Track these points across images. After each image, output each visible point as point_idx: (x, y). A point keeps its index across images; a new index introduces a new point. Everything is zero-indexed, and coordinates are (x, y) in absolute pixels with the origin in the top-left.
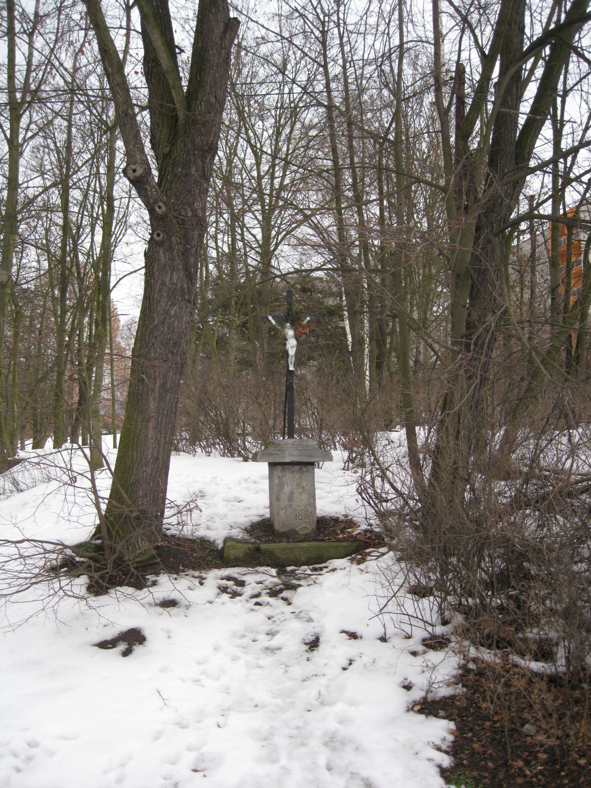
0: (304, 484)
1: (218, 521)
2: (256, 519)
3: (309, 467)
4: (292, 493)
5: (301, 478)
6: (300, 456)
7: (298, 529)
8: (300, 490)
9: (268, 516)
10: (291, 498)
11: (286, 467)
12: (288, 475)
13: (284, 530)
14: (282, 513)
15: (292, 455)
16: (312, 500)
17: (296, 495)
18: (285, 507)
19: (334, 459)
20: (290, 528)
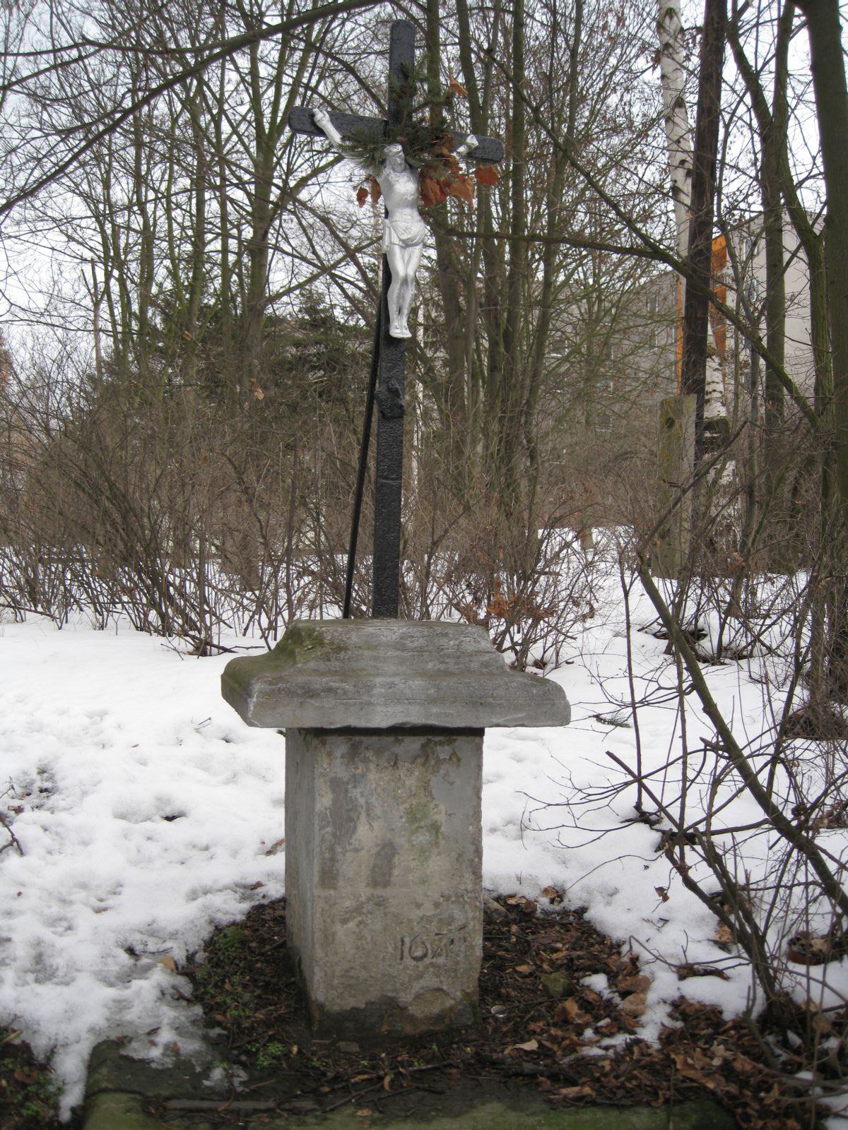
0: (439, 813)
1: (85, 920)
2: (234, 909)
3: (461, 741)
4: (387, 851)
5: (426, 787)
6: (433, 701)
7: (405, 998)
8: (423, 838)
9: (275, 890)
10: (381, 875)
11: (366, 740)
12: (373, 776)
13: (350, 1003)
14: (340, 931)
15: (396, 698)
16: (469, 877)
17: (404, 860)
18: (358, 910)
19: (576, 713)
20: (374, 994)
